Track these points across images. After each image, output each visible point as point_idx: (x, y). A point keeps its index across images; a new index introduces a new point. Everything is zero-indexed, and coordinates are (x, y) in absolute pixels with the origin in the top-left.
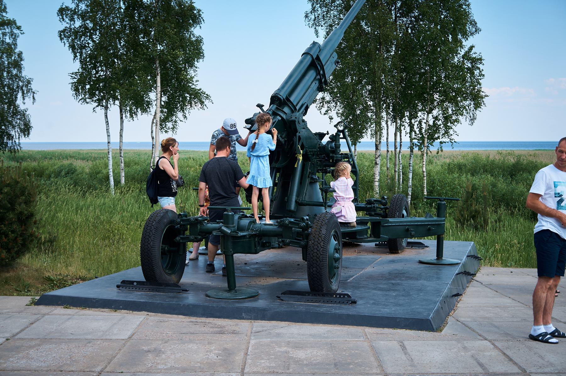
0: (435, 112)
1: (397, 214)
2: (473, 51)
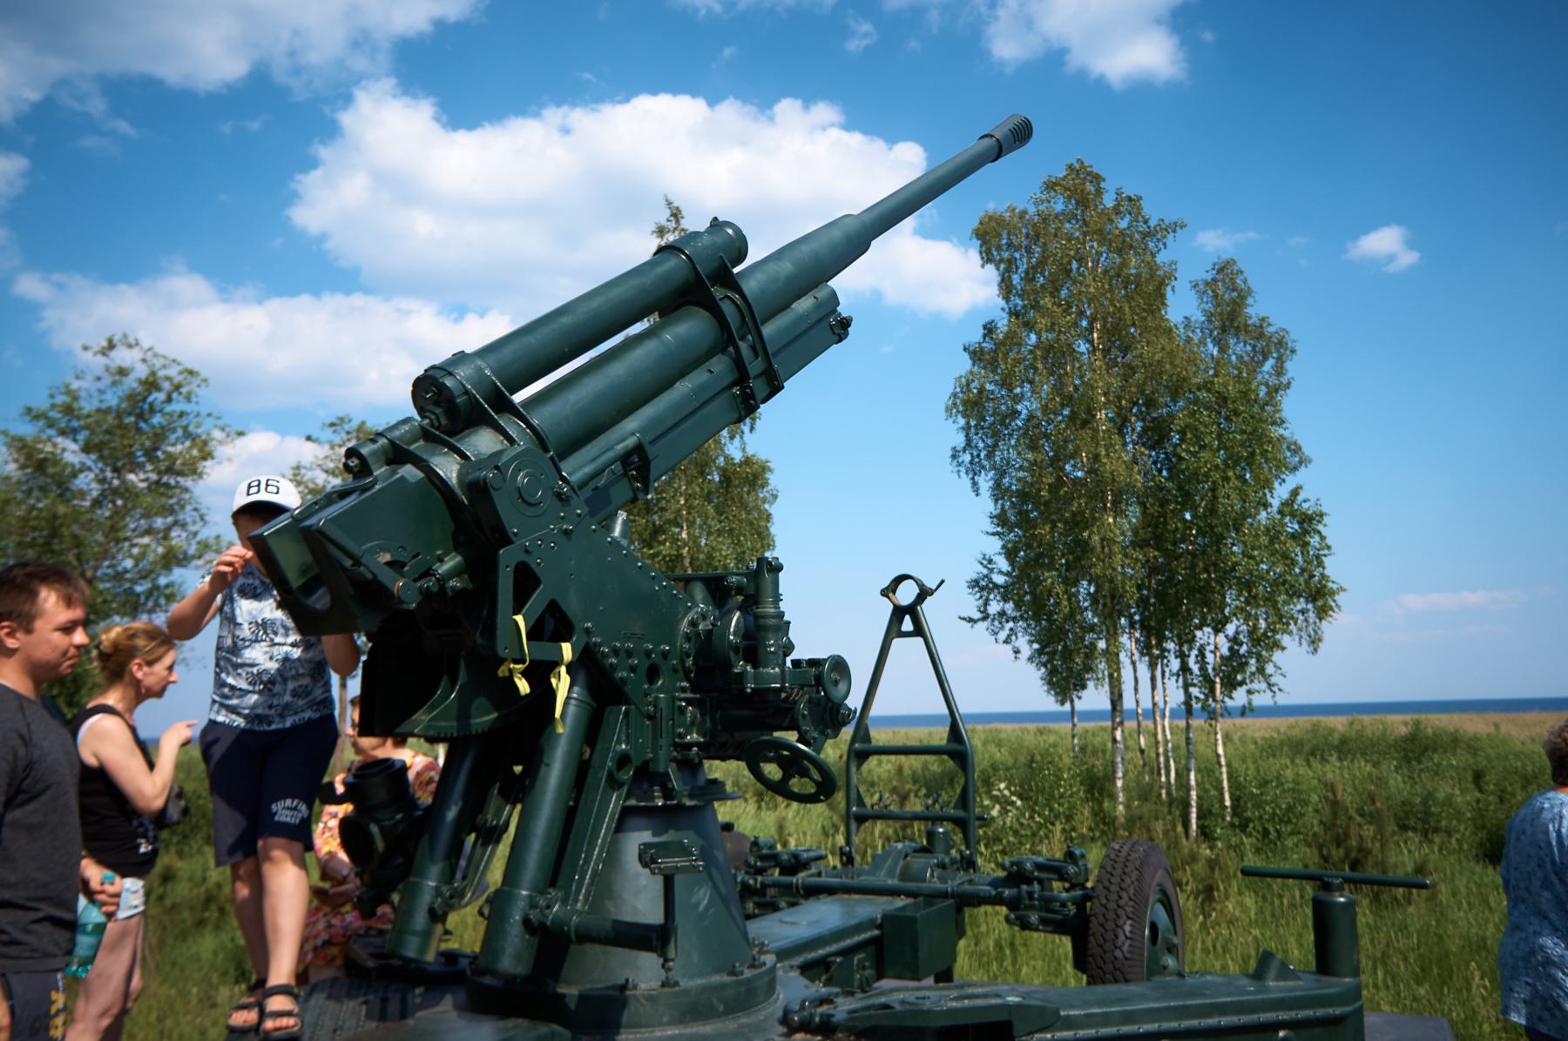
0: (1231, 629)
1: (1127, 928)
2: (1300, 498)
